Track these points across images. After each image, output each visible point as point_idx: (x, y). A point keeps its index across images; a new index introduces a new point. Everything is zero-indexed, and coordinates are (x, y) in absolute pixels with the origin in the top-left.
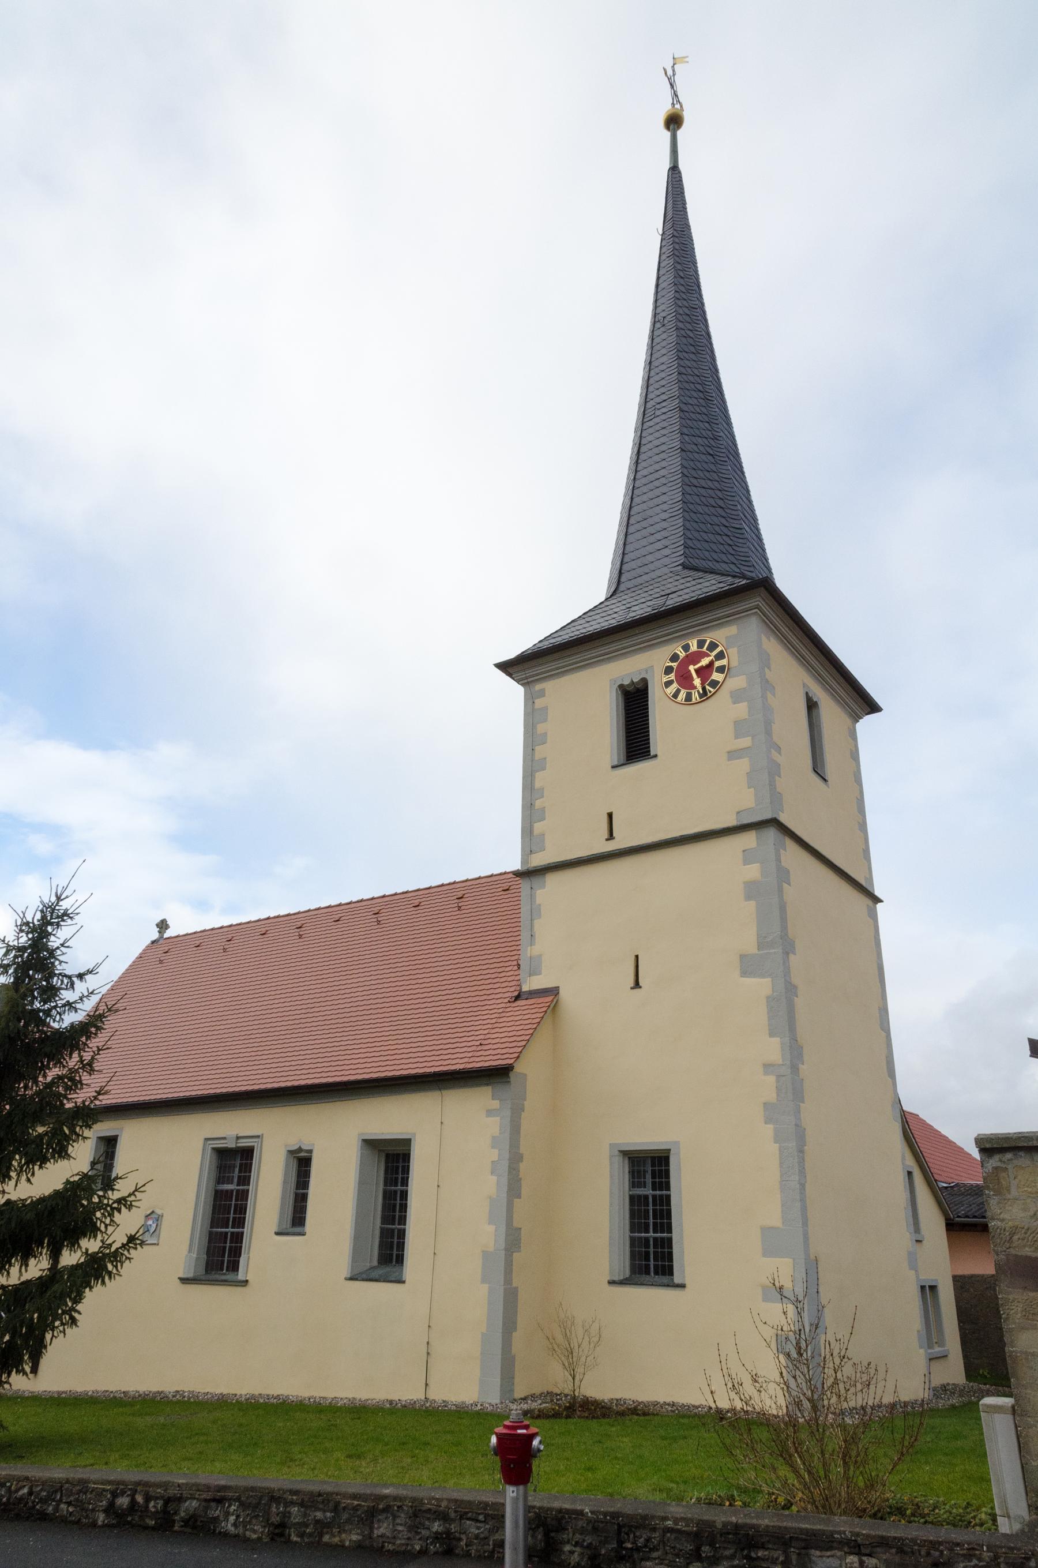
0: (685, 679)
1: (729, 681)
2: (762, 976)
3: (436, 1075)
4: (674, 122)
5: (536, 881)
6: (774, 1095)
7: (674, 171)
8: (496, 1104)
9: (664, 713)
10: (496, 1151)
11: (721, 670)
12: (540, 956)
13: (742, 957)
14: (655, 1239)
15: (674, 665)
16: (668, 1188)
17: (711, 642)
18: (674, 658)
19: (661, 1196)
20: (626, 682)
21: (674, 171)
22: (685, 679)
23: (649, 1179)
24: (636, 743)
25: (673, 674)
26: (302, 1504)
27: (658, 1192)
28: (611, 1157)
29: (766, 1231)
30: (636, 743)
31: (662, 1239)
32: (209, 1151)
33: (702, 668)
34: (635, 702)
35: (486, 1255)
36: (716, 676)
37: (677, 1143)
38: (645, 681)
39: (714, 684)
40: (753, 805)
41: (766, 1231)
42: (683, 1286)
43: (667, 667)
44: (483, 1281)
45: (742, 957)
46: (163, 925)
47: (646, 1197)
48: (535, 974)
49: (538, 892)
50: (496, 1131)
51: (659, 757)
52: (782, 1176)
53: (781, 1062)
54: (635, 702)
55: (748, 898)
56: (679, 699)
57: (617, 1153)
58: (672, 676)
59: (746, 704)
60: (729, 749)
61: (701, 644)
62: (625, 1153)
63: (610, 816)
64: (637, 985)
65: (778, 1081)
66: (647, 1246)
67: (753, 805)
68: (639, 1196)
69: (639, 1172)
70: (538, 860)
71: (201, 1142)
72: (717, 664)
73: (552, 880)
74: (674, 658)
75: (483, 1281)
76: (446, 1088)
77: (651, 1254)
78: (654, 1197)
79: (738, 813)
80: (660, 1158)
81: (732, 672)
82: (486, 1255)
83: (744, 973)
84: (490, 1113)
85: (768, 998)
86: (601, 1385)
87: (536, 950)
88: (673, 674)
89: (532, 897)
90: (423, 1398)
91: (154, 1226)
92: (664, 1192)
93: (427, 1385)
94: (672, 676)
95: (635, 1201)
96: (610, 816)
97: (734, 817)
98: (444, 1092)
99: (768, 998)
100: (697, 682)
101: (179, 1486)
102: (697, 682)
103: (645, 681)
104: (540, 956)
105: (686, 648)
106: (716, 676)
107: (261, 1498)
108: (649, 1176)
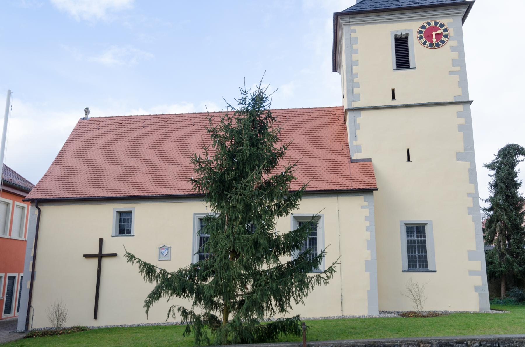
0: (429, 37)
1: (449, 42)
2: (467, 161)
3: (350, 190)
5: (356, 113)
8: (366, 204)
9: (416, 49)
11: (446, 36)
13: (457, 153)
15: (424, 30)
16: (424, 237)
17: (441, 24)
20: (399, 34)
22: (429, 37)
23: (415, 233)
24: (403, 60)
27: (420, 239)
28: (401, 225)
30: (403, 60)
32: (197, 219)
33: (438, 34)
34: (401, 44)
36: (443, 39)
38: (407, 34)
39: (443, 42)
40: (461, 94)
43: (420, 31)
45: (457, 153)
46: (87, 111)
47: (414, 240)
50: (367, 214)
51: (417, 69)
54: (401, 44)
55: (460, 131)
56: (426, 45)
59: (457, 53)
61: (436, 23)
62: (405, 224)
63: (393, 91)
65: (473, 200)
66: (416, 258)
67: (461, 94)
68: (411, 240)
69: (411, 231)
70: (356, 105)
71: (192, 216)
72: (444, 34)
73: (364, 113)
75: (366, 271)
81: (450, 38)
83: (458, 159)
84: (363, 207)
85: (469, 169)
86: (427, 307)
91: (166, 252)
92: (423, 239)
94: (422, 35)
99: (469, 169)
100: (434, 40)
102: (434, 40)
103: (407, 34)
104: (360, 146)
105: (429, 24)
106: (443, 39)
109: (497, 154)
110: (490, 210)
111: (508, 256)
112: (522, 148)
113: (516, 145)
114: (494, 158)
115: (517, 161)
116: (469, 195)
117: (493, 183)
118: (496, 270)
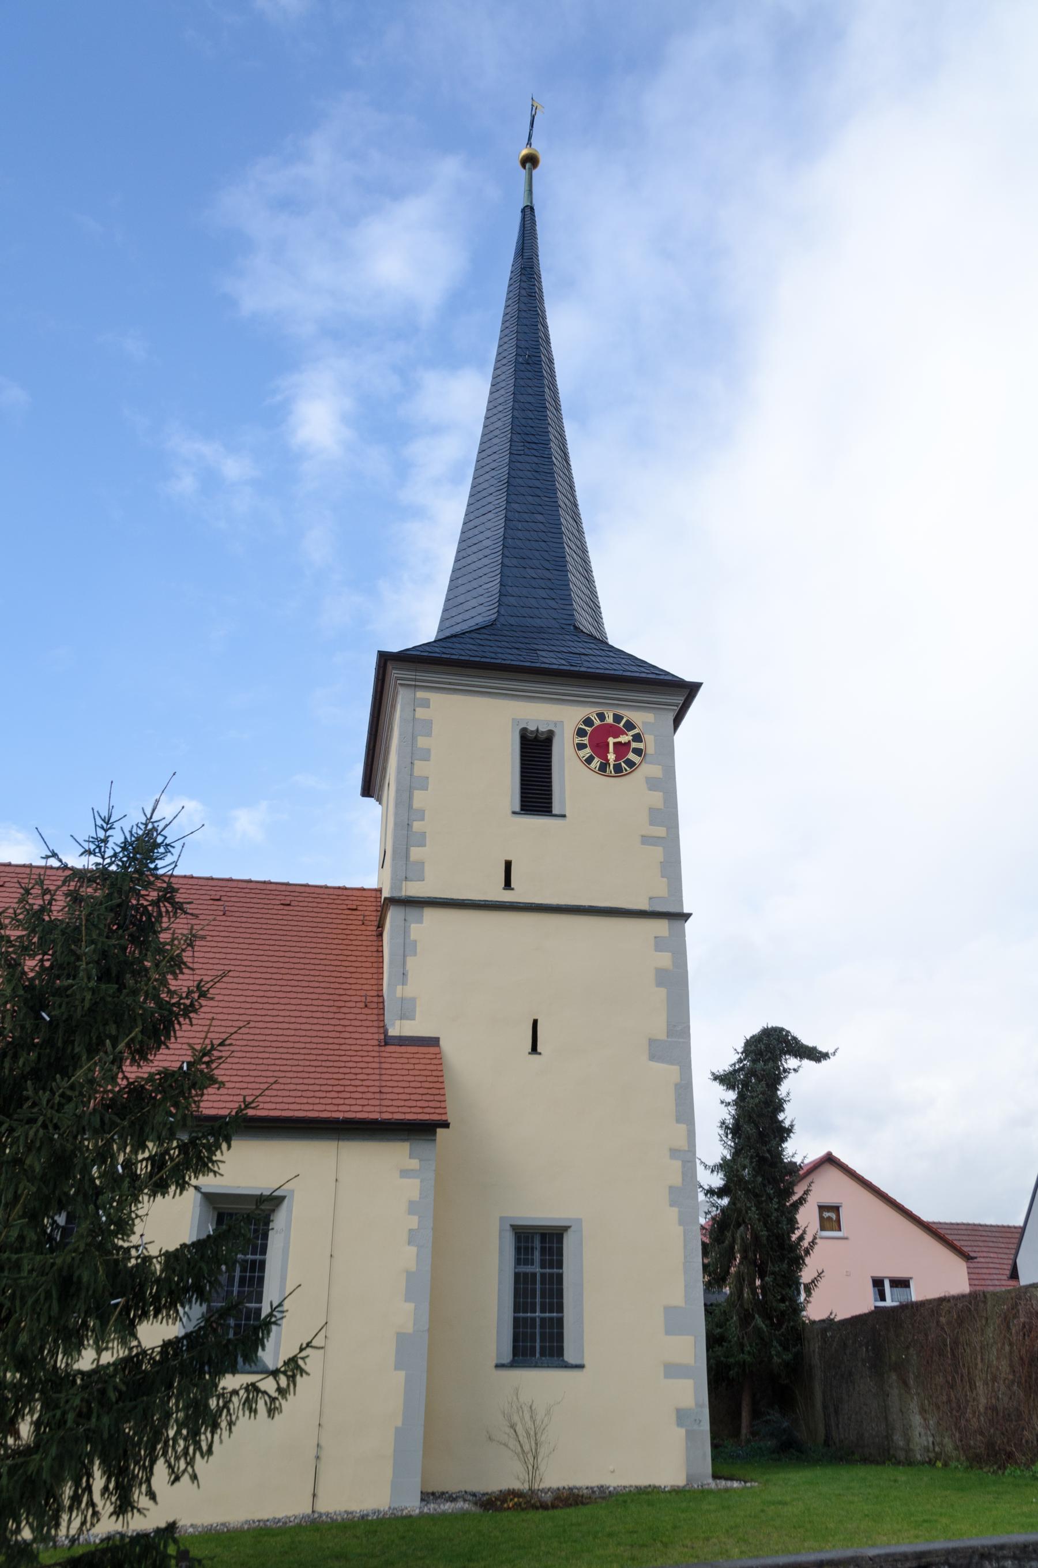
4: (530, 161)
5: (412, 913)
6: (680, 1180)
7: (528, 213)
8: (414, 1164)
10: (415, 1218)
11: (638, 752)
12: (413, 1000)
13: (651, 1042)
14: (543, 1320)
18: (588, 722)
19: (551, 1275)
20: (532, 728)
21: (528, 213)
22: (600, 748)
24: (536, 794)
25: (587, 738)
26: (1014, 1558)
27: (548, 1270)
28: (501, 1231)
29: (668, 1310)
30: (536, 794)
31: (551, 1319)
33: (620, 743)
34: (535, 752)
35: (401, 1338)
37: (579, 1221)
39: (631, 764)
41: (668, 1310)
42: (581, 1367)
44: (397, 1367)
45: (651, 1042)
47: (534, 1275)
48: (408, 1019)
49: (413, 926)
50: (415, 1195)
52: (685, 1257)
53: (686, 1148)
55: (659, 984)
57: (508, 1227)
58: (586, 740)
60: (643, 833)
61: (618, 718)
63: (508, 865)
64: (534, 1049)
65: (683, 1166)
66: (533, 1326)
68: (526, 1274)
69: (526, 1249)
70: (413, 889)
72: (634, 745)
73: (430, 915)
74: (588, 722)
75: (397, 1367)
76: (343, 1140)
77: (539, 1334)
78: (543, 1275)
79: (650, 898)
80: (551, 1235)
81: (648, 758)
82: (401, 1338)
83: (652, 1057)
84: (405, 1173)
87: (409, 990)
88: (587, 738)
89: (406, 932)
90: (310, 1511)
93: (314, 1495)
95: (520, 1280)
96: (508, 865)
97: (647, 901)
98: (341, 1143)
99: (676, 1085)
100: (611, 757)
101: (871, 1559)
104: (413, 1000)
106: (631, 756)
107: (971, 1557)
108: (537, 1254)
109: (740, 1050)
110: (721, 1193)
111: (759, 1321)
112: (795, 1038)
113: (782, 1029)
114: (736, 1057)
115: (785, 1071)
116: (674, 1153)
117: (730, 1121)
118: (732, 1360)
